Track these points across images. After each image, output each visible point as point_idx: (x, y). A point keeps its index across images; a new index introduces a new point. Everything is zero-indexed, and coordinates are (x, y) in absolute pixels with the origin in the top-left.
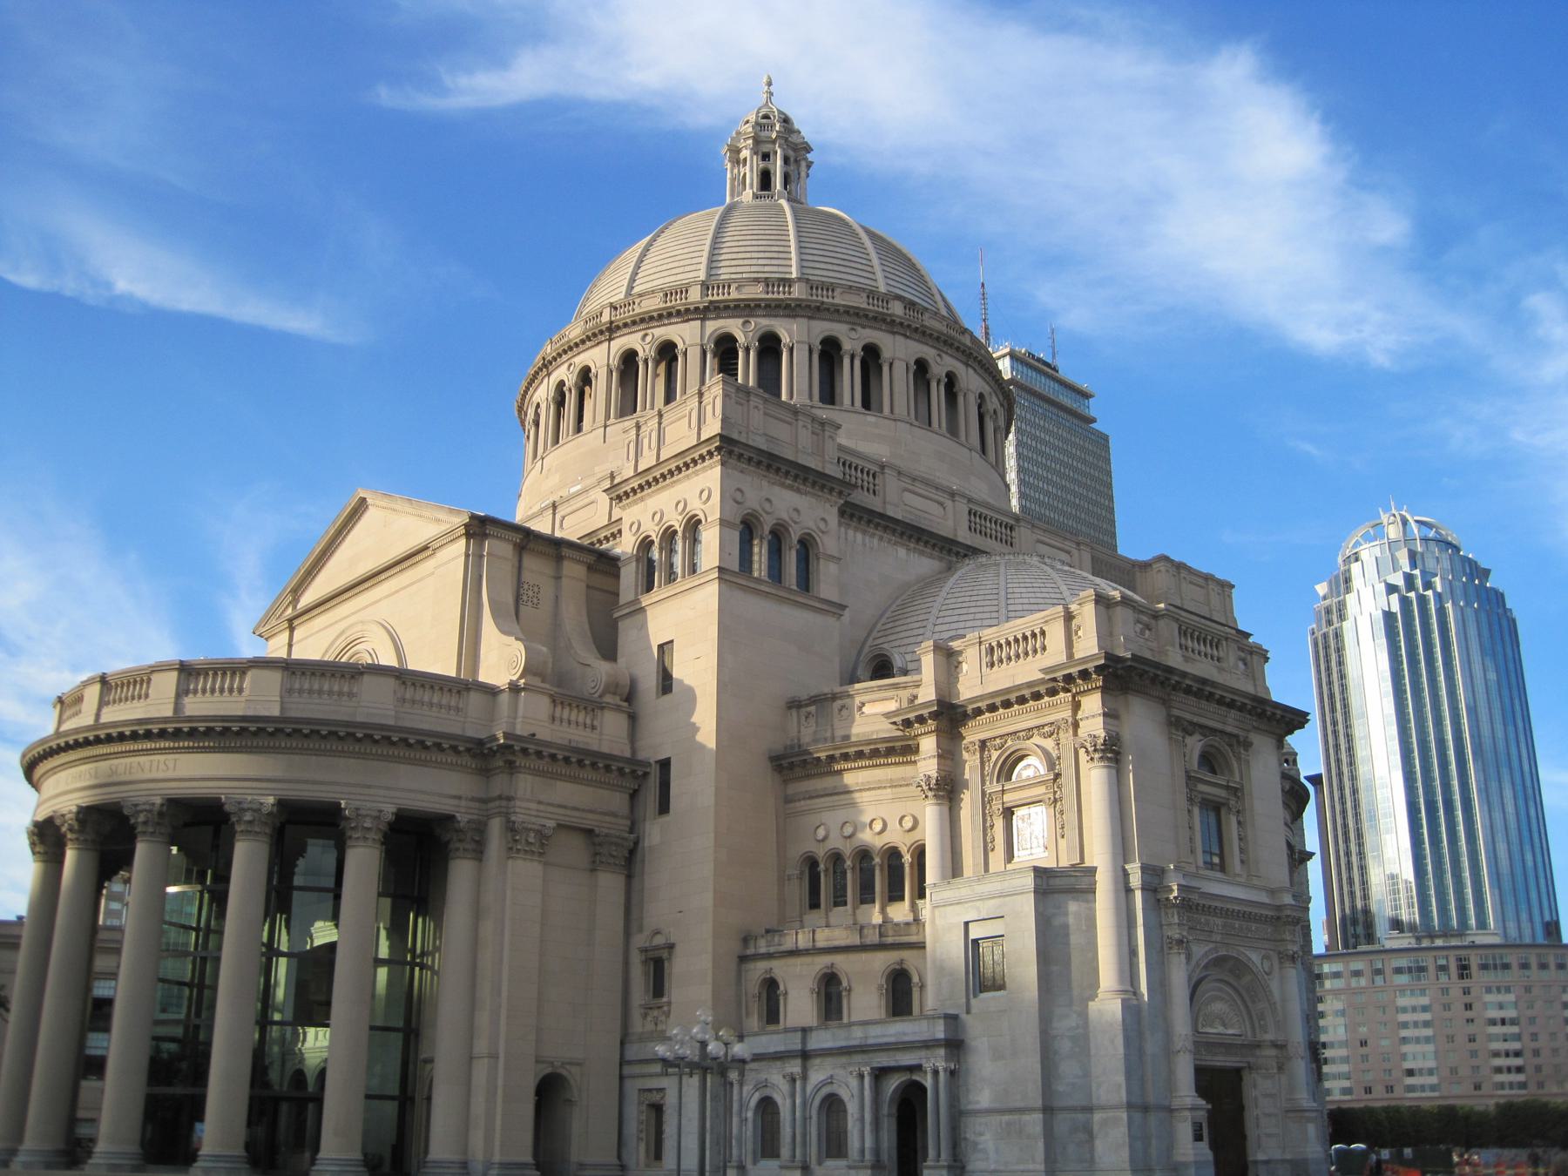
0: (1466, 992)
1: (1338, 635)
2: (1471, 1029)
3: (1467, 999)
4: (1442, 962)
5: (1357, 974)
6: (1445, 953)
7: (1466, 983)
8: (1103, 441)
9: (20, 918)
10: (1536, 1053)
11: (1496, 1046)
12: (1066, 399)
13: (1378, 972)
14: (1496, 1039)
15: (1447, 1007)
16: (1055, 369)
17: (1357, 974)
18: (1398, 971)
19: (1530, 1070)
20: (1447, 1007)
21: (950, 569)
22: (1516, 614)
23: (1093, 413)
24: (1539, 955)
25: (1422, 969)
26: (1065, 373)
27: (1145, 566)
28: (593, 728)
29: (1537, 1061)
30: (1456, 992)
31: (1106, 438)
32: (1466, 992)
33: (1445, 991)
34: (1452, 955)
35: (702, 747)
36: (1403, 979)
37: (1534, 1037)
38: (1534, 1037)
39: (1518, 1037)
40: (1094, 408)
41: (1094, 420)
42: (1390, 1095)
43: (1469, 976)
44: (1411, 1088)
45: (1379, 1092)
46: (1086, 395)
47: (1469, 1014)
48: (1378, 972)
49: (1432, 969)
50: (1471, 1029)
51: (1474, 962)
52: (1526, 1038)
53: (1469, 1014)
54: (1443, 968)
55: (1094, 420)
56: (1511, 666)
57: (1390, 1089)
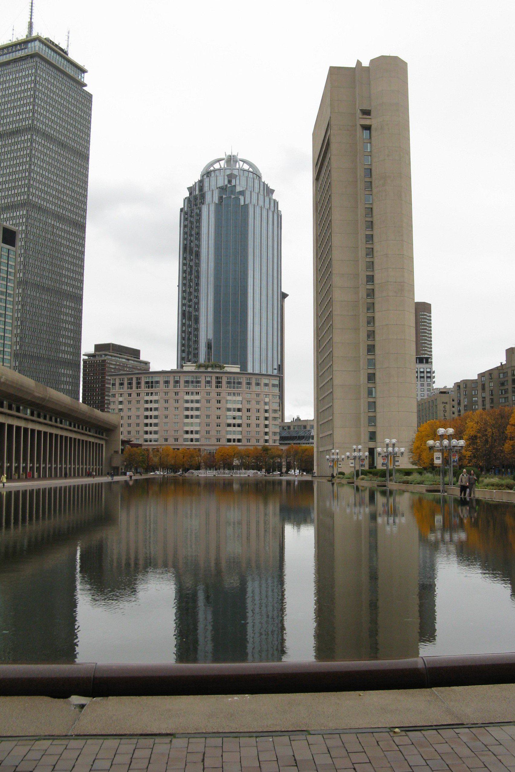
0: (219, 394)
2: (219, 412)
3: (219, 398)
4: (208, 379)
6: (210, 375)
8: (89, 97)
9: (375, 467)
12: (71, 71)
15: (208, 401)
16: (66, 53)
19: (142, 402)
20: (208, 401)
22: (283, 214)
23: (85, 82)
24: (256, 379)
25: (198, 382)
26: (72, 56)
30: (213, 395)
32: (219, 394)
33: (208, 393)
34: (214, 376)
35: (117, 363)
37: (249, 418)
40: (86, 78)
41: (85, 85)
42: (176, 443)
43: (221, 387)
44: (186, 440)
45: (171, 441)
46: (84, 71)
47: (219, 405)
49: (203, 382)
50: (219, 412)
51: (224, 380)
53: (219, 405)
54: (208, 382)
55: (85, 85)
57: (176, 440)
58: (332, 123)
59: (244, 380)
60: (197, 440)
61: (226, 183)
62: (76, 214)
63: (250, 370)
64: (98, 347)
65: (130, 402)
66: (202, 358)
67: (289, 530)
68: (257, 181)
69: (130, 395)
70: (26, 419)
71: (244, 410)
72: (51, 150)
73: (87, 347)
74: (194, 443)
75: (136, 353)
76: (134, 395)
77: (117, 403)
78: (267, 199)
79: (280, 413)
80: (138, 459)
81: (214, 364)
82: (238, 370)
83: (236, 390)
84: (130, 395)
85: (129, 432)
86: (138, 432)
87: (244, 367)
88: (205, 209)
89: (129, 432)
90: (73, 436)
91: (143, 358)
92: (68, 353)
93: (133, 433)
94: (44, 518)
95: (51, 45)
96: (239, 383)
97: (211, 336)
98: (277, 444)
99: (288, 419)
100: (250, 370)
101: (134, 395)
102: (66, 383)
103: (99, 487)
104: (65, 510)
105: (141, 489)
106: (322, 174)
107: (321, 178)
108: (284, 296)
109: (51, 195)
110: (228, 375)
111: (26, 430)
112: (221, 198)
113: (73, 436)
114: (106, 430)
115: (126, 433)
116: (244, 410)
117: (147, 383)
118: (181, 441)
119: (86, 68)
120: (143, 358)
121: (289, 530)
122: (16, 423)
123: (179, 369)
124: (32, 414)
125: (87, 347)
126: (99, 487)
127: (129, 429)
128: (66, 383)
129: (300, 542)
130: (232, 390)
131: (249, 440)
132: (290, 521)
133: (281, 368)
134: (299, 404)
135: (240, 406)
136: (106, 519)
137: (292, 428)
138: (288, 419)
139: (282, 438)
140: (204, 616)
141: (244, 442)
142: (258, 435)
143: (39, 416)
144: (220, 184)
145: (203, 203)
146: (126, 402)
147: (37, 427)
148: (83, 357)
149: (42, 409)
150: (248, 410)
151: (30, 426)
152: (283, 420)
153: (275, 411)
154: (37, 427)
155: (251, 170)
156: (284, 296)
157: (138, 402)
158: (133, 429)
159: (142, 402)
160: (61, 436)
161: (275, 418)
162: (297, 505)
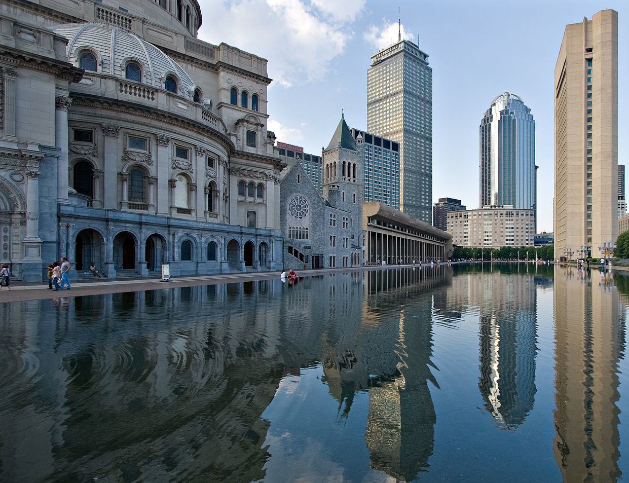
1: (490, 125)
3: (501, 222)
5: (475, 215)
7: (502, 218)
8: (431, 70)
10: (517, 236)
11: (509, 234)
13: (480, 215)
14: (507, 232)
17: (475, 215)
18: (485, 215)
19: (463, 225)
21: (96, 21)
27: (218, 48)
28: (153, 99)
29: (517, 238)
30: (499, 221)
31: (431, 70)
33: (496, 220)
36: (487, 217)
38: (517, 236)
39: (513, 236)
40: (429, 60)
44: (485, 244)
46: (426, 56)
48: (480, 215)
50: (502, 230)
52: (515, 236)
53: (502, 226)
54: (496, 214)
56: (532, 160)
57: (480, 244)
58: (567, 61)
59: (515, 213)
60: (491, 244)
61: (504, 108)
62: (427, 133)
63: (517, 207)
64: (440, 200)
65: (456, 226)
66: (493, 203)
67: (540, 291)
68: (521, 106)
69: (456, 222)
70: (406, 235)
71: (515, 228)
72: (413, 101)
73: (435, 200)
74: (489, 245)
75: (459, 202)
76: (458, 222)
77: (450, 226)
78: (527, 116)
79: (534, 229)
80: (460, 252)
81: (499, 205)
82: (512, 208)
83: (511, 218)
84: (456, 222)
85: (456, 241)
86: (461, 241)
87: (514, 206)
88: (493, 123)
89: (456, 241)
90: (429, 242)
91: (462, 204)
92: (425, 203)
93: (458, 241)
94: (402, 285)
95: (412, 45)
96: (513, 214)
97: (497, 191)
98: (533, 245)
99: (539, 232)
100: (517, 207)
101: (458, 222)
102: (425, 218)
103: (426, 269)
104: (423, 279)
105: (459, 270)
106: (561, 91)
107: (560, 96)
108: (537, 167)
109: (415, 125)
110: (507, 210)
111: (406, 240)
112: (501, 118)
113: (429, 242)
114: (446, 239)
115: (454, 241)
116: (515, 228)
117: (465, 216)
118: (482, 245)
119: (428, 54)
120: (462, 204)
121: (540, 291)
122: (401, 236)
123: (481, 208)
124: (409, 232)
125: (435, 200)
126: (426, 269)
127: (456, 239)
128: (425, 218)
129: (545, 297)
130: (509, 218)
131: (517, 244)
132: (539, 284)
133: (535, 206)
134: (545, 224)
135: (513, 226)
136: (446, 283)
137: (541, 237)
138: (539, 232)
139: (535, 243)
140: (495, 332)
141: (515, 245)
142: (523, 241)
143: (412, 233)
144: (501, 109)
145: (491, 121)
146: (454, 226)
147: (411, 238)
148: (433, 205)
149: (414, 230)
150: (518, 228)
151: (408, 238)
152: (536, 233)
153: (531, 228)
154: (411, 238)
155: (518, 99)
156: (537, 167)
157: (461, 225)
158: (458, 239)
159: (463, 225)
160: (423, 243)
161: (531, 232)
162: (544, 276)
